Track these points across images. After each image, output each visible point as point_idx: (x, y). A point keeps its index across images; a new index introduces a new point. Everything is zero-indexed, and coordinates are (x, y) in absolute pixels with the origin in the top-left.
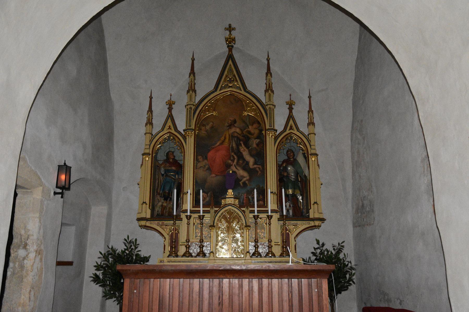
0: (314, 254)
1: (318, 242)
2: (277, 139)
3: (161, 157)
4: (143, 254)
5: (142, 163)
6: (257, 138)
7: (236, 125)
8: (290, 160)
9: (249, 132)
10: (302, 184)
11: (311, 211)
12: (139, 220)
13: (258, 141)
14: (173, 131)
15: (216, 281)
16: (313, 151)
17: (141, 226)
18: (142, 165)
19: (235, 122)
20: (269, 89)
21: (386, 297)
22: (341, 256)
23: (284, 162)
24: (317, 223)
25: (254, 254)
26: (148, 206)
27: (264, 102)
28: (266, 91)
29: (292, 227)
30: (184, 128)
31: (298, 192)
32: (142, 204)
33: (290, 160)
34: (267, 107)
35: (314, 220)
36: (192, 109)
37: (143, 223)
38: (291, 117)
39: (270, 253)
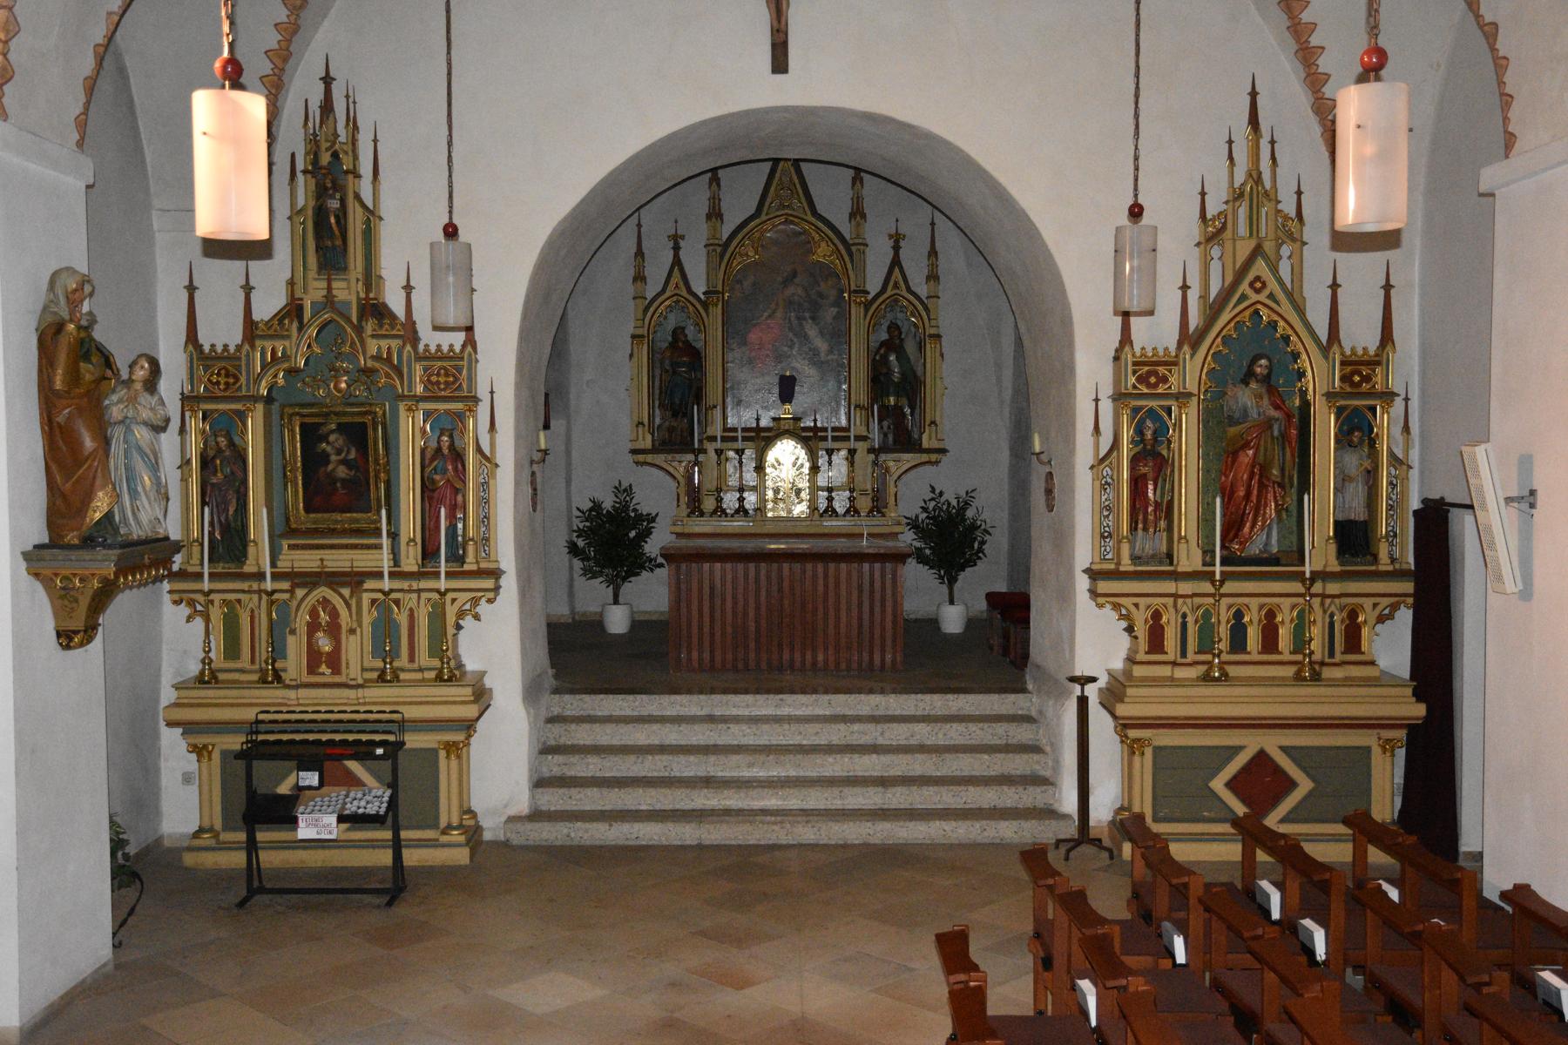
0: (924, 509)
1: (933, 490)
3: (664, 338)
4: (645, 509)
6: (833, 305)
7: (797, 280)
8: (894, 344)
9: (821, 295)
10: (912, 387)
11: (925, 437)
12: (634, 452)
13: (834, 310)
14: (684, 293)
15: (775, 566)
16: (933, 331)
17: (637, 463)
18: (631, 356)
19: (794, 274)
20: (857, 213)
21: (452, 663)
22: (970, 513)
23: (883, 344)
24: (934, 457)
25: (826, 511)
27: (847, 237)
28: (852, 215)
29: (891, 464)
30: (704, 289)
31: (904, 401)
33: (894, 344)
34: (854, 249)
35: (929, 451)
36: (720, 251)
37: (641, 458)
38: (896, 262)
39: (852, 510)
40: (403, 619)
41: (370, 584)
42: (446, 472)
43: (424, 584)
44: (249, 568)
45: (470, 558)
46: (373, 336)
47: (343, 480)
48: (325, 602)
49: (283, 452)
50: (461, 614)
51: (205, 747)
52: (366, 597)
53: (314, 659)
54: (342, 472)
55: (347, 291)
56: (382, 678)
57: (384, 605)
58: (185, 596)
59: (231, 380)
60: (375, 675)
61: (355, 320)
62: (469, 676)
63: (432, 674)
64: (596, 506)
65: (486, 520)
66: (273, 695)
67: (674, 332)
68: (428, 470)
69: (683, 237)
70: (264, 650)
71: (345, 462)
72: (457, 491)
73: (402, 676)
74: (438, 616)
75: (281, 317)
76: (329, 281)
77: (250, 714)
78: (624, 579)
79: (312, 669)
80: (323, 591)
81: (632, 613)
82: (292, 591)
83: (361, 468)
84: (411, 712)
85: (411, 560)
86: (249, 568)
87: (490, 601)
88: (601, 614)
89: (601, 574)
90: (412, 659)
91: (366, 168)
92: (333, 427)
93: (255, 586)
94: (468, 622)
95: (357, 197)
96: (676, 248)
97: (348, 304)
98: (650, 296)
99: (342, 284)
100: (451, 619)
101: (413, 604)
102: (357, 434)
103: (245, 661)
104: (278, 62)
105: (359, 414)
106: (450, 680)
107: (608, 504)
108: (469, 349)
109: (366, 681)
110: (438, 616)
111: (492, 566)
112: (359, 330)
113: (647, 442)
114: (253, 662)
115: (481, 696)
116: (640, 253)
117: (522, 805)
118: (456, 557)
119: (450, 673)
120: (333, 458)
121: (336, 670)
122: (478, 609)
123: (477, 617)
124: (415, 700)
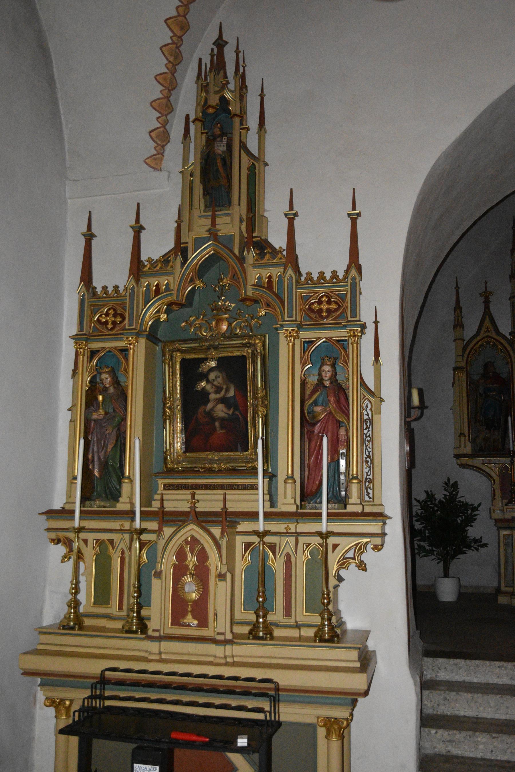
2: (466, 350)
5: (454, 379)
12: (457, 456)
18: (453, 384)
21: (334, 619)
26: (467, 437)
32: (459, 436)
37: (464, 460)
40: (277, 565)
41: (244, 526)
42: (329, 409)
43: (303, 527)
44: (122, 506)
45: (354, 498)
46: (255, 266)
47: (222, 419)
48: (194, 541)
49: (164, 388)
50: (343, 563)
51: (62, 701)
52: (240, 540)
53: (180, 607)
54: (221, 411)
55: (230, 225)
56: (253, 635)
57: (260, 551)
58: (61, 535)
59: (119, 319)
60: (246, 630)
61: (236, 251)
62: (349, 637)
63: (310, 632)
64: (430, 496)
65: (369, 459)
66: (138, 646)
67: (486, 366)
68: (308, 403)
69: (491, 293)
70: (130, 598)
71: (223, 400)
72: (339, 424)
73: (277, 632)
74: (319, 564)
75: (165, 260)
76: (214, 212)
77: (95, 667)
78: (453, 558)
79: (176, 621)
80: (192, 530)
81: (460, 587)
82: (159, 532)
83: (238, 406)
84: (285, 679)
85: (288, 499)
86: (122, 506)
87: (377, 548)
88: (434, 586)
89: (431, 552)
90: (287, 613)
91: (253, 122)
92: (213, 364)
93: (127, 525)
94: (351, 573)
95: (243, 146)
96: (487, 303)
97: (231, 238)
98: (467, 339)
99: (228, 219)
100: (333, 568)
101: (290, 549)
102: (235, 369)
103: (113, 609)
104: (177, 30)
105: (238, 346)
106: (330, 640)
107: (440, 495)
108: (353, 272)
109: (236, 636)
110: (319, 564)
111: (376, 510)
112: (242, 260)
113: (468, 449)
114: (120, 608)
115: (366, 661)
116: (458, 307)
117: (75, 333)
118: (338, 498)
119: (332, 634)
120: (213, 396)
121: (203, 623)
122: (364, 557)
123: (362, 566)
124: (292, 663)
